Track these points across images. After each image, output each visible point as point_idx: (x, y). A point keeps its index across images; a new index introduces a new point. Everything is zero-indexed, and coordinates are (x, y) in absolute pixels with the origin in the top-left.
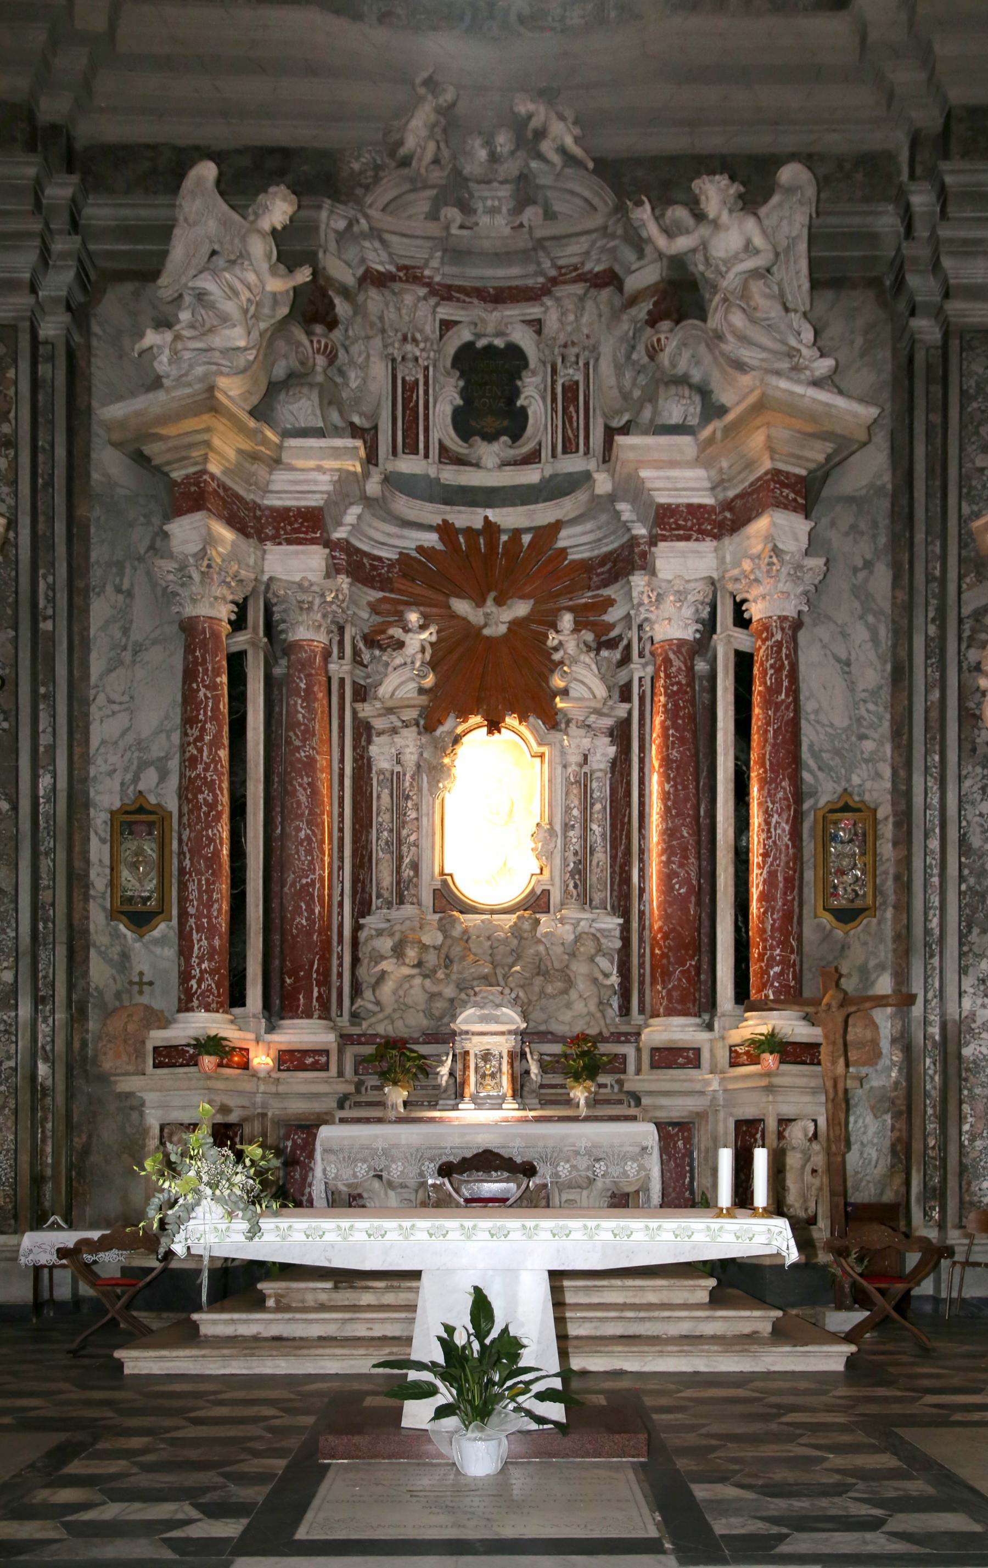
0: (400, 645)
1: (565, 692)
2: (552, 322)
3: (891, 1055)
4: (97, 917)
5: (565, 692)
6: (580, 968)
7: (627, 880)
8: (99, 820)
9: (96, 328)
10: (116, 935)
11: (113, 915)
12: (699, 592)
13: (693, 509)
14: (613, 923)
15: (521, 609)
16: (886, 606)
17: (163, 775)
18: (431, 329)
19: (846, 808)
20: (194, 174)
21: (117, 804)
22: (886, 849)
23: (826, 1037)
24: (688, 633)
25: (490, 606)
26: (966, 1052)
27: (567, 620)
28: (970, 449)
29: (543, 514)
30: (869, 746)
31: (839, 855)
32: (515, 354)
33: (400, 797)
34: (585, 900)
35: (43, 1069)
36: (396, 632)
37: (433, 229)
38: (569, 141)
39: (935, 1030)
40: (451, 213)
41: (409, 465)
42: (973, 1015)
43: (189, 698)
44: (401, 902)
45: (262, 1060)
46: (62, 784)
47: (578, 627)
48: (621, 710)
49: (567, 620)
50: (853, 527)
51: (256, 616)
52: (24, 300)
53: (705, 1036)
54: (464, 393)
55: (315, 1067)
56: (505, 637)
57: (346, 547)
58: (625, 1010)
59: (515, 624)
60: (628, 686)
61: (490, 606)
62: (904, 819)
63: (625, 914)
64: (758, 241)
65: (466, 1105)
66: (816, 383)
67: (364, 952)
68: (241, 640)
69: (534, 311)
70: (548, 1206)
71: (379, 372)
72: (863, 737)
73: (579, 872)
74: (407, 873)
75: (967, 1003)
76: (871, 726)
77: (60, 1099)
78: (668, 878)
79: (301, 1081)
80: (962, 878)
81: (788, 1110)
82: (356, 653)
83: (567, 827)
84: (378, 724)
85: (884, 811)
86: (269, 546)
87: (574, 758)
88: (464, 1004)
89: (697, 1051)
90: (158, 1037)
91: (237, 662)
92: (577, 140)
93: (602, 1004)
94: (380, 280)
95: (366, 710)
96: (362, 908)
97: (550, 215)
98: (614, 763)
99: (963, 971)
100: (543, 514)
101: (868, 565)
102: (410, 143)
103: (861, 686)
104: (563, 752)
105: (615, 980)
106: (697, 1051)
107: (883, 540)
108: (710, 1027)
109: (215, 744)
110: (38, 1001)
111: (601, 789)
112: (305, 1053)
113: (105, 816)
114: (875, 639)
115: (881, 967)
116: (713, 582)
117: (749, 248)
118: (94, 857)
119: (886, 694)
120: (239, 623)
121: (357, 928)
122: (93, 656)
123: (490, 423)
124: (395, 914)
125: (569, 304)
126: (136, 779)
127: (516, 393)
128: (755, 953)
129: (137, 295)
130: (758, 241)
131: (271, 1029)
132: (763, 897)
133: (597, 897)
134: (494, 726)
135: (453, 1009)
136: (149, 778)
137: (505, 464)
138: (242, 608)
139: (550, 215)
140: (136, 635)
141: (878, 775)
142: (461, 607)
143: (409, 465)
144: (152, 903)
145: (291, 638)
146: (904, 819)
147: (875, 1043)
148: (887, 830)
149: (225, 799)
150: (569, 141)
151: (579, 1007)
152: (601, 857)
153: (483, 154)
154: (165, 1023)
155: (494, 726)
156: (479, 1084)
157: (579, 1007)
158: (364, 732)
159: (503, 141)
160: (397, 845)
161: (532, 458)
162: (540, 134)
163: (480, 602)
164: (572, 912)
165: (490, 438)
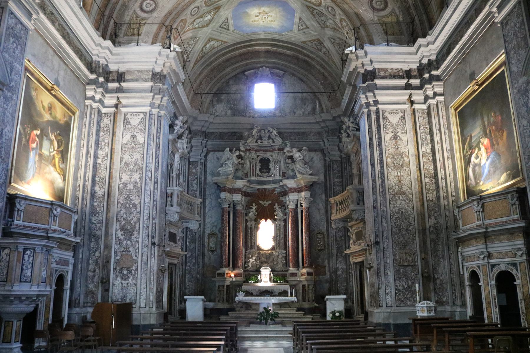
0: (252, 208)
1: (276, 215)
2: (274, 156)
3: (328, 273)
4: (206, 250)
5: (276, 215)
6: (279, 260)
7: (286, 245)
8: (207, 235)
9: (208, 159)
10: (209, 254)
11: (208, 251)
12: (295, 202)
13: (295, 188)
14: (284, 252)
15: (270, 202)
16: (324, 200)
17: (216, 228)
18: (256, 156)
19: (319, 233)
20: (226, 149)
21: (209, 233)
22: (326, 239)
23: (314, 272)
24: (294, 208)
25: (265, 202)
26: (338, 273)
27: (276, 204)
28: (334, 178)
29: (273, 186)
30: (323, 223)
31: (319, 241)
32: (268, 159)
33: (252, 232)
34: (280, 248)
35: (198, 276)
36: (252, 207)
37: (256, 144)
38: (276, 133)
39: (334, 269)
40: (259, 141)
41: (253, 178)
42: (339, 267)
43: (222, 220)
44: (252, 249)
45: (233, 275)
46: (202, 230)
47: (278, 205)
48: (285, 217)
49: (276, 204)
50: (319, 188)
51: (232, 206)
52: (199, 157)
53: (298, 271)
54: (261, 166)
55: (240, 276)
56: (267, 206)
57: (244, 192)
58: (286, 266)
59: (269, 204)
60: (286, 213)
61: (265, 202)
62: (328, 234)
63: (286, 250)
64: (301, 156)
65: (262, 282)
66: (310, 175)
67: (247, 256)
68: (230, 209)
69: (271, 153)
70: (137, 45)
71: (248, 163)
72: (322, 221)
73: (279, 244)
74: (253, 244)
75: (338, 265)
76: (323, 219)
77: (201, 281)
78: (292, 246)
79: (239, 279)
80: (336, 245)
81: (309, 283)
82: (245, 208)
83: (277, 236)
84: (249, 219)
85: (325, 233)
86: (233, 194)
87: (278, 225)
88: (262, 267)
89: (297, 274)
90: (218, 272)
91: (229, 212)
92: (277, 133)
93: (283, 265)
94: (250, 150)
95: (247, 218)
96: (246, 250)
97: (274, 142)
98: (284, 225)
99: (337, 260)
100: (273, 186)
101: (321, 194)
102: (254, 134)
103: (321, 213)
104: (276, 224)
105: (285, 261)
106: (297, 274)
107: (324, 190)
108: (298, 269)
109: (226, 227)
110: (198, 265)
111: (282, 230)
112: (239, 274)
113: (207, 234)
114: (323, 206)
115: (326, 259)
116: (297, 200)
117: (300, 156)
118: (206, 241)
119: (325, 214)
120: (229, 207)
121: (245, 253)
122: (206, 209)
123: (265, 170)
124: (251, 251)
125: (276, 154)
126: (212, 229)
127: (269, 166)
128: (304, 258)
129: (214, 154)
130: (301, 156)
131: (233, 270)
132: (305, 250)
133: (282, 247)
134: (266, 220)
135: (260, 267)
136: (214, 228)
137: (267, 176)
138: (230, 204)
139: (274, 142)
140: (213, 205)
141: (324, 227)
142: (261, 202)
143: (253, 178)
144: (214, 249)
145: (237, 208)
146: (328, 234)
147: (325, 272)
148: (326, 236)
149: (227, 234)
150: (276, 133)
151: (279, 266)
152: (282, 241)
153: (264, 132)
154: (219, 269)
155: (266, 220)
156: (352, 229)
157: (279, 266)
158: (247, 221)
159: (266, 131)
160: (251, 239)
161: (271, 176)
162: (271, 132)
163: (264, 201)
164: (278, 250)
165: (265, 173)
